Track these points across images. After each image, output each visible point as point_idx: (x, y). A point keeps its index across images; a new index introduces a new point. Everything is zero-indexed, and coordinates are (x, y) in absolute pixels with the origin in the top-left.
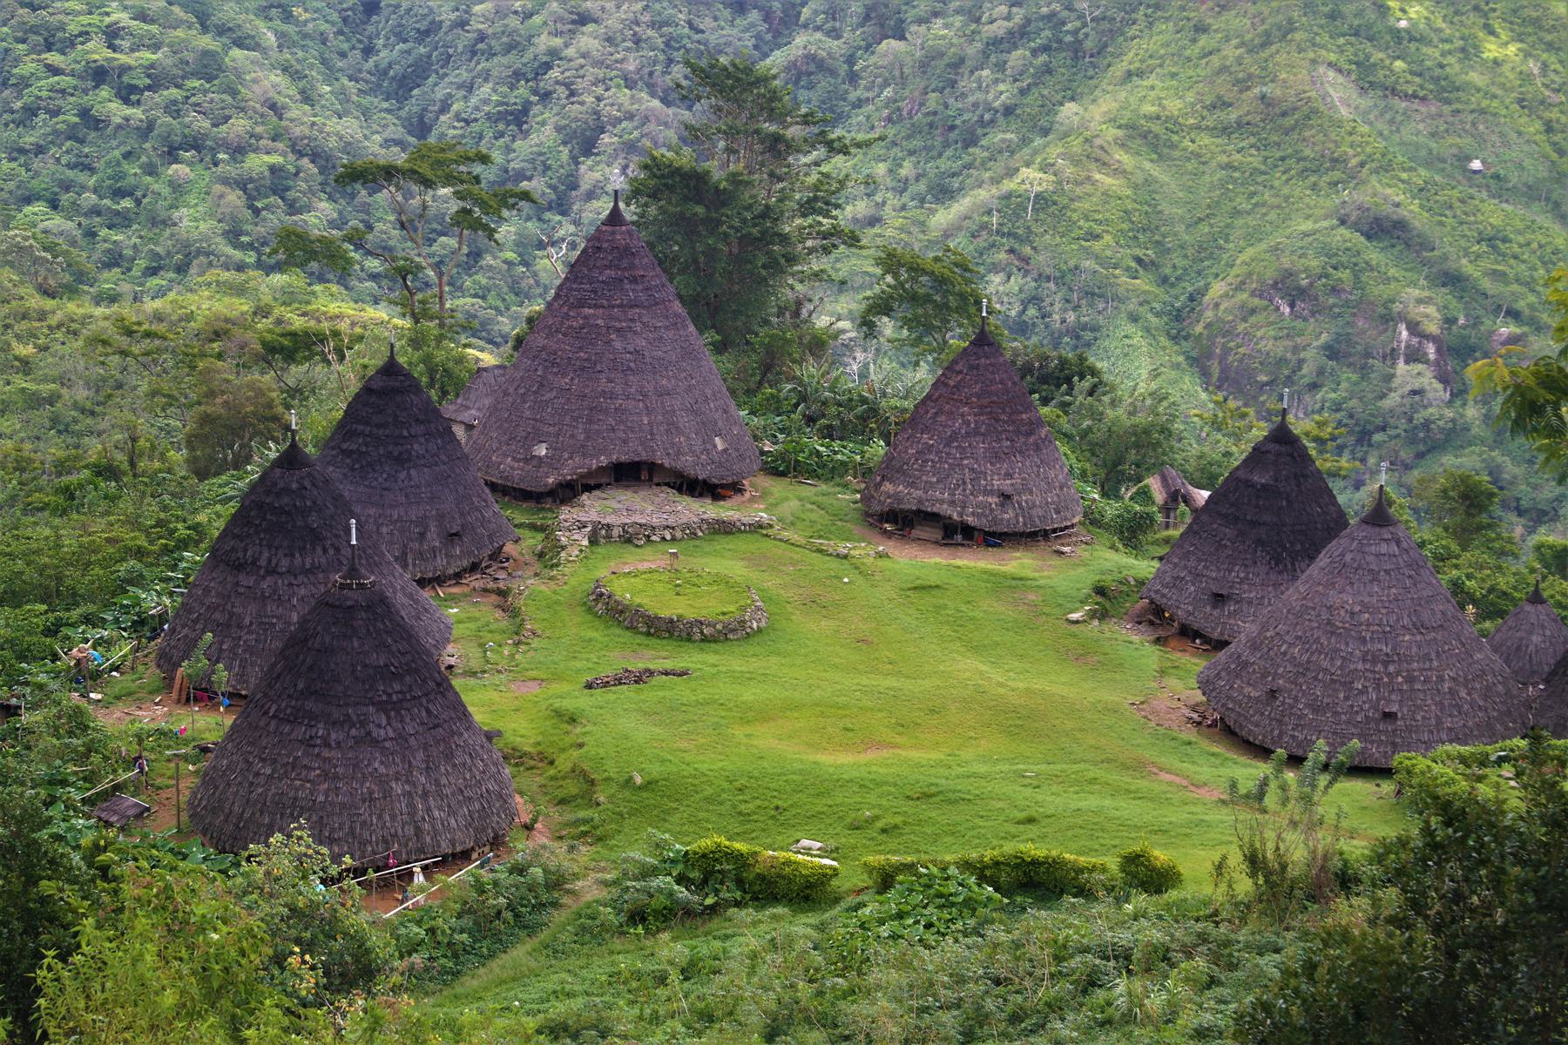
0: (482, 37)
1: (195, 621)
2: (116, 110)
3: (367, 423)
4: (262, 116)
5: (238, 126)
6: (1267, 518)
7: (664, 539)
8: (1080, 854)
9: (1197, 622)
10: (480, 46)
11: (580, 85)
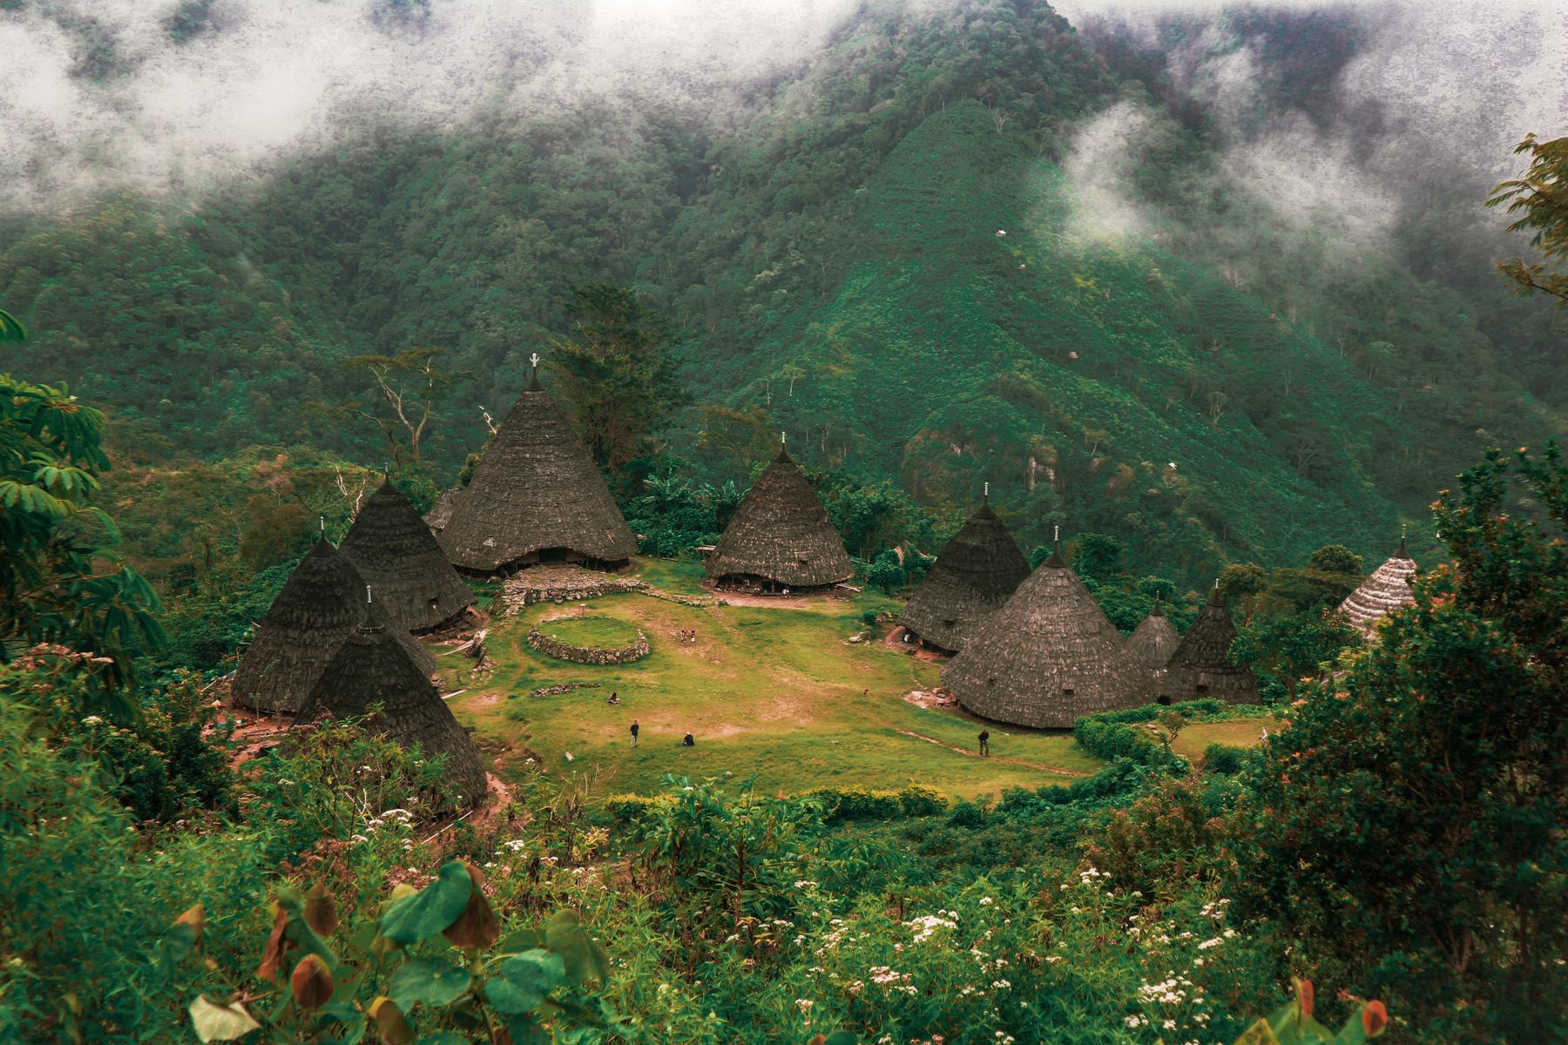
0: (427, 290)
1: (258, 663)
2: (184, 345)
3: (371, 527)
5: (266, 351)
6: (978, 568)
7: (575, 598)
8: (503, 959)
9: (937, 639)
11: (492, 319)
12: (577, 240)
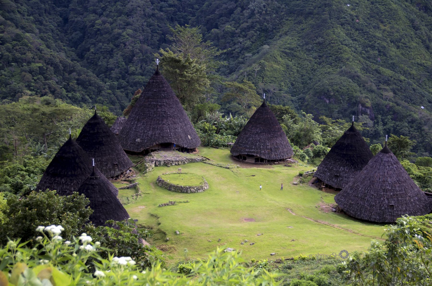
0: (99, 30)
4: (36, 53)
10: (98, 32)
12: (164, 9)
